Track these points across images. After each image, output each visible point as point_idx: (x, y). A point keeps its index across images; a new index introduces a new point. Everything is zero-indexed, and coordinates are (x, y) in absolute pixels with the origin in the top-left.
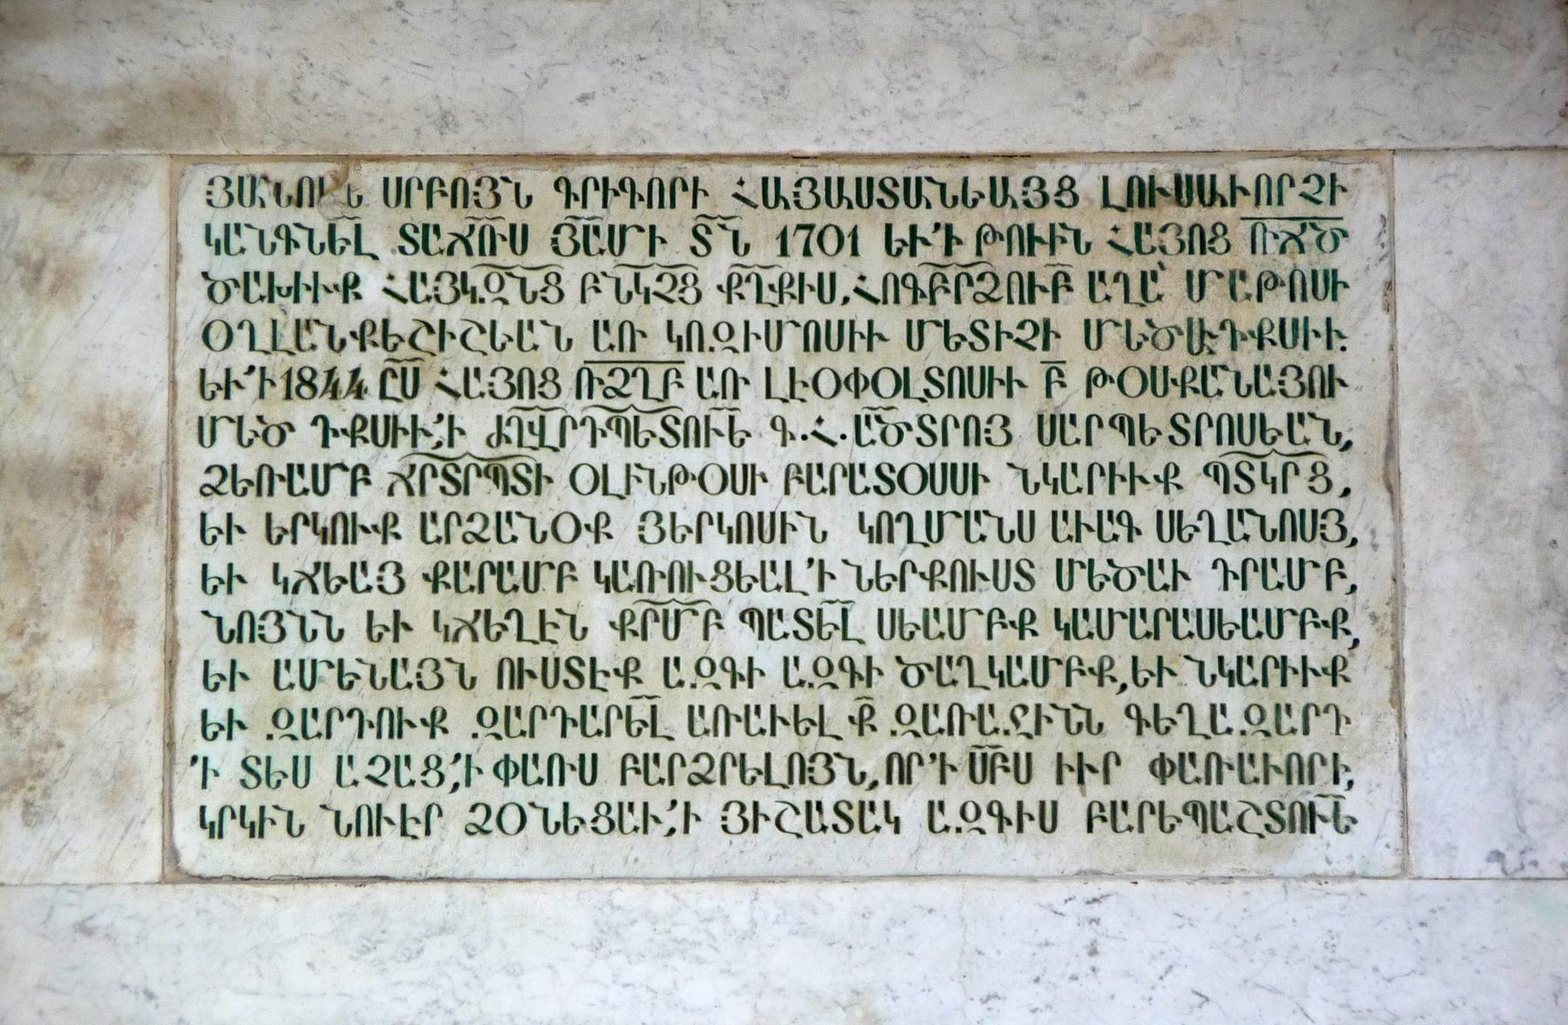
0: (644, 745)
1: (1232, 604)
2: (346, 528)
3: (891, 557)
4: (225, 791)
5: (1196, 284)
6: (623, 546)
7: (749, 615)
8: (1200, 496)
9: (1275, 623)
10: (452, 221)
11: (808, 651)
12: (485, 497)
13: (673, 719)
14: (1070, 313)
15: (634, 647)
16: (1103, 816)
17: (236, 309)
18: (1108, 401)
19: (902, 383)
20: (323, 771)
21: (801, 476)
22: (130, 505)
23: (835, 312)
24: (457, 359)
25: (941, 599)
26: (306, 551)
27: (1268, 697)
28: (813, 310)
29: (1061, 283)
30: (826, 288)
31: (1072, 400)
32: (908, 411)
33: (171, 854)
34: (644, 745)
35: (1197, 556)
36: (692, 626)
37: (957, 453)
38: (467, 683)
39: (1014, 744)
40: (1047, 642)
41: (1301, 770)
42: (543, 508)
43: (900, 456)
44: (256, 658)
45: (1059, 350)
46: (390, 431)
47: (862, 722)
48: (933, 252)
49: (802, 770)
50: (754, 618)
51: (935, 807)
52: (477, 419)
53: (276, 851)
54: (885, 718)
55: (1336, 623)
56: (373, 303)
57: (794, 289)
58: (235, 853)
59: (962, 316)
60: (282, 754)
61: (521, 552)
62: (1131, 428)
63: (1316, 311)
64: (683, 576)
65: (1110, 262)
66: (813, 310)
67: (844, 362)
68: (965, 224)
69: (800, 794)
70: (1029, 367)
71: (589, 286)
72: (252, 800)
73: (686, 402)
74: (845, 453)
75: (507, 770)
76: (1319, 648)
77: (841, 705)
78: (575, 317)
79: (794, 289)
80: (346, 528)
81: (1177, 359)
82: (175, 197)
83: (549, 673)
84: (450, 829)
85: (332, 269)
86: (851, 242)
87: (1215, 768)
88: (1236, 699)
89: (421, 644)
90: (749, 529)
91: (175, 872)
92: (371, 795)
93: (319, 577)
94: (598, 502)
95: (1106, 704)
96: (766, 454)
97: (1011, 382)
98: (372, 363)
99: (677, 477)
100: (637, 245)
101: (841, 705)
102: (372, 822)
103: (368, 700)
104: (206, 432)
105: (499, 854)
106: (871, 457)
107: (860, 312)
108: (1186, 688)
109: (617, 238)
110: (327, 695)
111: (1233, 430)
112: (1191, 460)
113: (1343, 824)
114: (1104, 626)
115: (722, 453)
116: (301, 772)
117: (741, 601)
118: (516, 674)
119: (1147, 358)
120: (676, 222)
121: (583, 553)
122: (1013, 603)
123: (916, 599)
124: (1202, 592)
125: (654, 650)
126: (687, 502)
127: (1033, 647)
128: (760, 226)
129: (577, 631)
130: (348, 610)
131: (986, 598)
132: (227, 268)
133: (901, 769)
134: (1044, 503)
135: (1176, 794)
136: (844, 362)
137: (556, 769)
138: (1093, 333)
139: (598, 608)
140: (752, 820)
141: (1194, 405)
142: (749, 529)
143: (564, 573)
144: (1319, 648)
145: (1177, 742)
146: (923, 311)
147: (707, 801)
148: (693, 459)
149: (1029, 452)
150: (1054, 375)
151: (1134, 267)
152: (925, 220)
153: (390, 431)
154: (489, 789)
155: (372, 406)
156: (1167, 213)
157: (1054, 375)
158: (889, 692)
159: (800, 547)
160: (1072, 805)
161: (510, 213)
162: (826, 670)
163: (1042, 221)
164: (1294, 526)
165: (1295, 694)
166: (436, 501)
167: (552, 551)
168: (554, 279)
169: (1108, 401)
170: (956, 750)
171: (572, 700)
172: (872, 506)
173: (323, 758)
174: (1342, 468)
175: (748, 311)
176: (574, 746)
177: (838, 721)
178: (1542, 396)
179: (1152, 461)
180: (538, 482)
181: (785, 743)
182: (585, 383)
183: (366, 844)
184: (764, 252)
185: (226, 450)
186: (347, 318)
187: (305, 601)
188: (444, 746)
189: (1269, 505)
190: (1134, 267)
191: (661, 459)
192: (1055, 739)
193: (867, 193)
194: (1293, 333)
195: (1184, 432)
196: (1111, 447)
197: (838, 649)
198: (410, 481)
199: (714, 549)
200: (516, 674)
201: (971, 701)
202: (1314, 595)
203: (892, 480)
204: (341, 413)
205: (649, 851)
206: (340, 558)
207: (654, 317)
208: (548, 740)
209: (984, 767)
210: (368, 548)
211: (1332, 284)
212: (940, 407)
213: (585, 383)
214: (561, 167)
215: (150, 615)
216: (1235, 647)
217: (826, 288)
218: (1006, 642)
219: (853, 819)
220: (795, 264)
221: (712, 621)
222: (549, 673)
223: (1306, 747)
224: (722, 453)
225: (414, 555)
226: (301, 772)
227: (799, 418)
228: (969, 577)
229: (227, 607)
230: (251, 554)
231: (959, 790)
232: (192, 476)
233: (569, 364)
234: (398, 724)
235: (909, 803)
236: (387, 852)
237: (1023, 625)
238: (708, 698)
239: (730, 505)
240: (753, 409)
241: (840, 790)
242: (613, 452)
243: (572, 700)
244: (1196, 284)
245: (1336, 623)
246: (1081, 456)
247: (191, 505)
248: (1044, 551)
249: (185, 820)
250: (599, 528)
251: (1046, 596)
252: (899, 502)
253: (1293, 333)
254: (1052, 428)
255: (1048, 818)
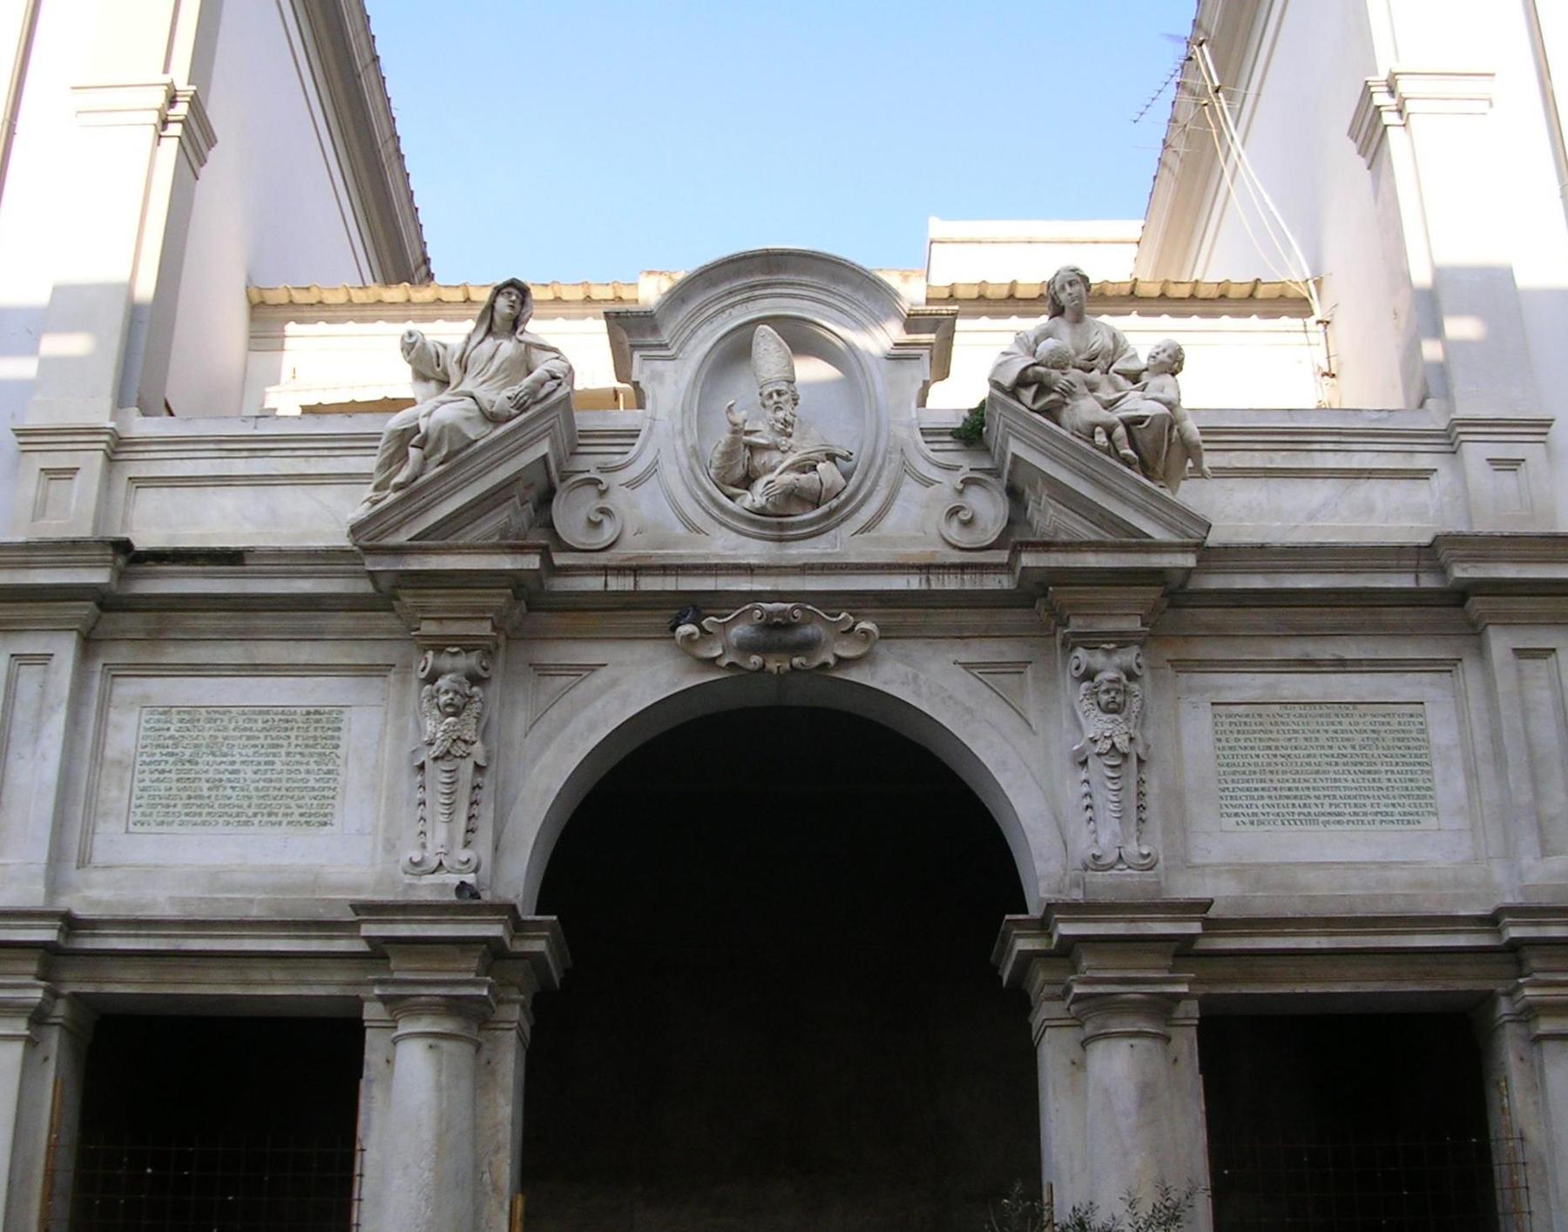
0: (211, 810)
1: (317, 785)
2: (163, 771)
3: (257, 777)
4: (138, 818)
5: (316, 729)
6: (210, 775)
7: (232, 787)
8: (313, 766)
9: (323, 789)
10: (187, 717)
11: (242, 793)
12: (188, 766)
13: (216, 806)
14: (293, 734)
15: (210, 793)
16: (290, 823)
17: (149, 733)
18: (299, 750)
19: (263, 746)
20: (155, 814)
21: (243, 762)
22: (127, 768)
23: (252, 734)
24: (186, 742)
25: (266, 784)
26: (156, 775)
27: (322, 802)
28: (248, 733)
29: (292, 729)
30: (251, 729)
31: (291, 749)
32: (263, 751)
33: (127, 828)
34: (211, 810)
35: (311, 777)
36: (221, 789)
37: (271, 759)
38: (181, 799)
39: (276, 811)
40: (283, 792)
41: (325, 815)
42: (197, 768)
43: (260, 759)
44: (145, 794)
45: (291, 740)
46: (172, 754)
47: (249, 806)
48: (270, 723)
49: (238, 815)
50: (233, 788)
51: (260, 822)
52: (188, 752)
53: (145, 828)
54: (253, 806)
55: (334, 789)
56: (172, 732)
57: (245, 729)
58: (139, 828)
59: (274, 734)
60: (149, 811)
61: (193, 776)
62: (301, 754)
63: (336, 734)
64: (221, 780)
65: (301, 725)
66: (248, 733)
67: (253, 742)
68: (277, 718)
69: (237, 819)
70: (285, 743)
71: (210, 729)
72: (143, 819)
73: (225, 749)
74: (250, 759)
75: (187, 814)
76: (331, 793)
77: (246, 803)
78: (207, 734)
79: (245, 729)
80: (163, 771)
81: (311, 742)
82: (141, 713)
83: (196, 797)
84: (175, 825)
85: (166, 726)
86: (256, 721)
87: (311, 815)
88: (315, 802)
89: (174, 792)
90: (233, 772)
91: (127, 832)
92: (162, 819)
93: (158, 780)
94: (207, 767)
95: (292, 803)
96: (238, 759)
97: (282, 746)
98: (170, 742)
99: (222, 763)
100: (219, 722)
101: (246, 803)
102: (162, 823)
103: (164, 802)
104: (142, 754)
105: (183, 829)
106: (256, 759)
107: (256, 734)
108: (307, 800)
109: (215, 721)
110: (157, 801)
111: (320, 754)
112: (312, 760)
113: (332, 825)
114: (294, 789)
115: (230, 758)
116: (151, 814)
117: (231, 785)
118: (189, 797)
119: (306, 742)
120: (226, 718)
121: (204, 776)
122: (278, 785)
123: (262, 784)
124: (312, 784)
125: (214, 793)
126: (223, 767)
127: (281, 793)
128: (240, 718)
129: (201, 790)
130: (162, 786)
131: (273, 784)
132: (148, 726)
133: (255, 815)
134: (286, 767)
135: (303, 819)
136: (253, 742)
137: (195, 814)
138: (297, 737)
139: (206, 786)
140: (228, 823)
141: (313, 750)
142: (233, 772)
143: (200, 779)
144: (331, 793)
145: (303, 811)
146: (267, 733)
147: (221, 820)
148: (224, 759)
149: (284, 758)
150: (289, 744)
151: (305, 726)
152: (269, 717)
153: (172, 754)
154: (183, 818)
155: (170, 750)
156: (312, 716)
157: (289, 744)
158: (255, 801)
159: (242, 775)
160: (285, 821)
161: (198, 717)
162: (244, 796)
163: (290, 718)
164: (329, 772)
165: (326, 802)
166: (179, 767)
167: (198, 776)
168: (204, 728)
169: (299, 750)
170: (265, 811)
171: (199, 802)
172: (255, 768)
173: (155, 811)
174: (338, 761)
175: (237, 734)
176: (198, 810)
177: (245, 806)
178: (1139, 845)
179: (305, 760)
180: (197, 763)
181: (236, 810)
182: (207, 746)
183: (160, 827)
184: (241, 723)
185: (144, 758)
186: (167, 734)
187: (155, 784)
188: (176, 810)
189: (325, 768)
190: (305, 726)
191: (219, 759)
192: (283, 810)
193: (260, 713)
194: (332, 738)
195: (311, 755)
196: (298, 758)
197: (246, 793)
198: (175, 763)
199: (226, 776)
200: (189, 797)
201: (269, 803)
202: (332, 785)
203: (259, 763)
204: (165, 751)
205: (209, 829)
206: (162, 776)
207: (220, 734)
208: (194, 809)
209: (270, 815)
210: (166, 775)
211: (339, 729)
212: (270, 750)
213: (207, 746)
214: (1498, 1083)
215: (128, 787)
216: (316, 793)
217: (251, 729)
218: (276, 793)
219: (246, 823)
220: (246, 725)
221: (225, 788)
222: (196, 797)
223: (326, 811)
224: (230, 758)
225: (174, 776)
226: (151, 814)
227: (244, 752)
228: (271, 781)
229: (142, 785)
230: (147, 776)
231: (266, 819)
232: (138, 763)
233: (204, 742)
234: (168, 806)
235: (256, 821)
236: (164, 829)
237: (279, 789)
238: (223, 802)
239: (230, 768)
240: (236, 751)
241: (244, 819)
242: (211, 758)
243: (199, 802)
244: (316, 729)
245: (334, 789)
246: (293, 759)
247: (138, 767)
248: (285, 776)
249: (130, 823)
250: (206, 772)
251: (285, 784)
252: (260, 767)
253: (332, 738)
254: (288, 754)
255: (280, 823)
